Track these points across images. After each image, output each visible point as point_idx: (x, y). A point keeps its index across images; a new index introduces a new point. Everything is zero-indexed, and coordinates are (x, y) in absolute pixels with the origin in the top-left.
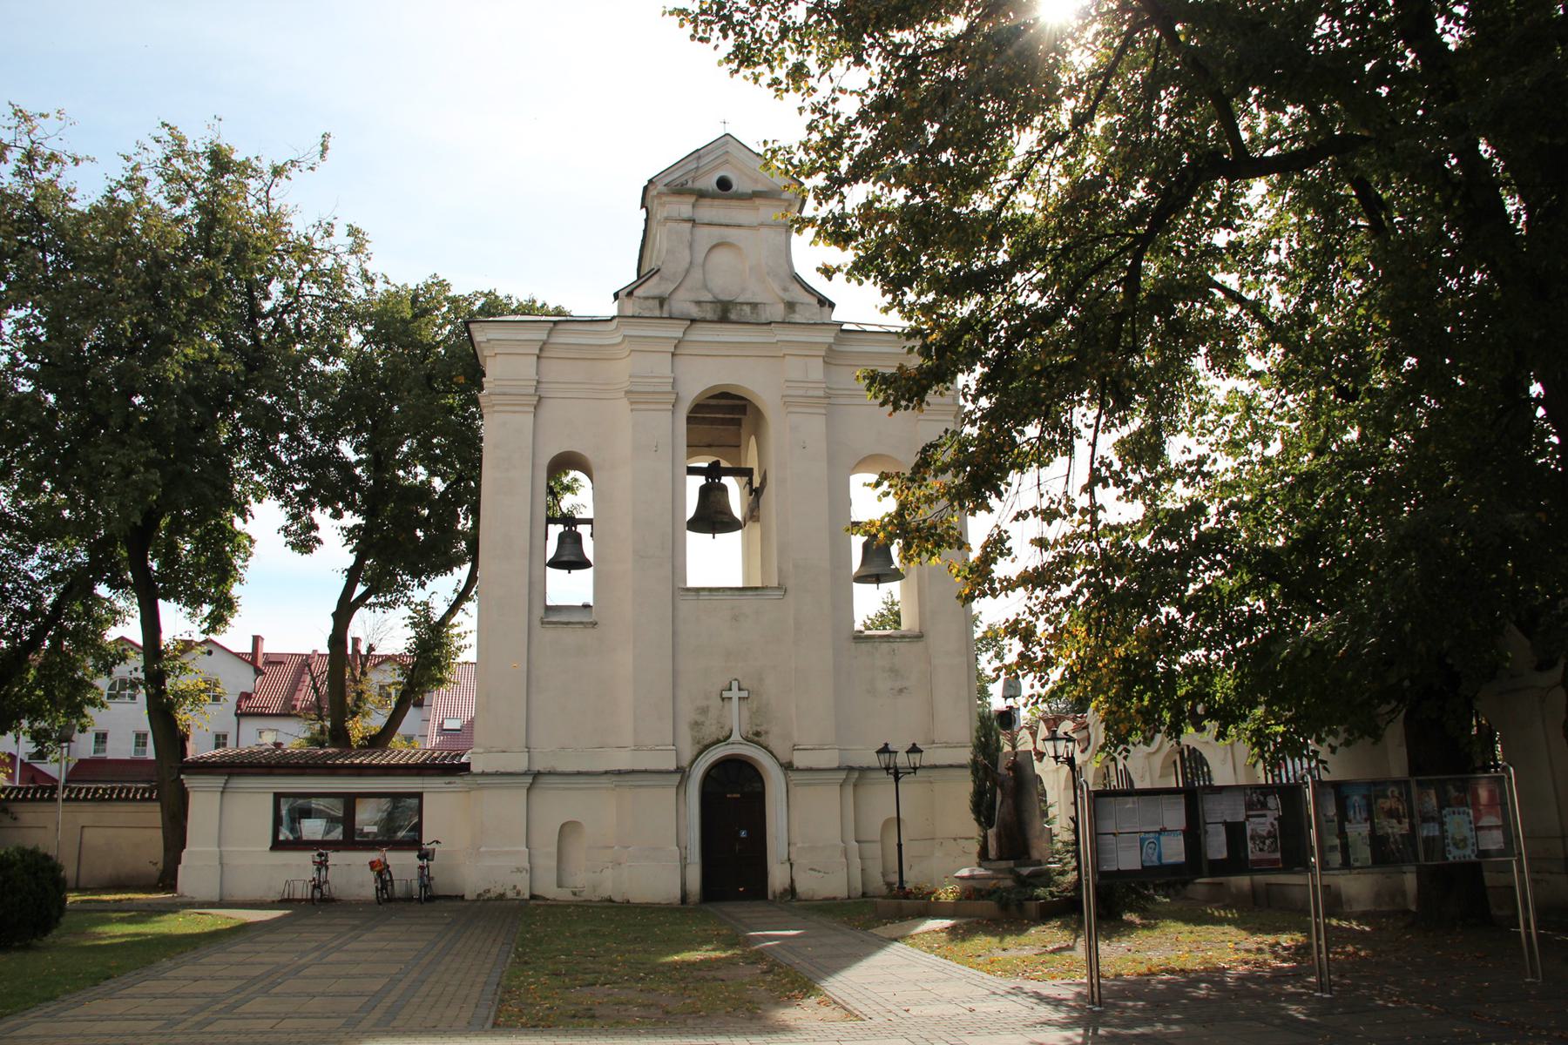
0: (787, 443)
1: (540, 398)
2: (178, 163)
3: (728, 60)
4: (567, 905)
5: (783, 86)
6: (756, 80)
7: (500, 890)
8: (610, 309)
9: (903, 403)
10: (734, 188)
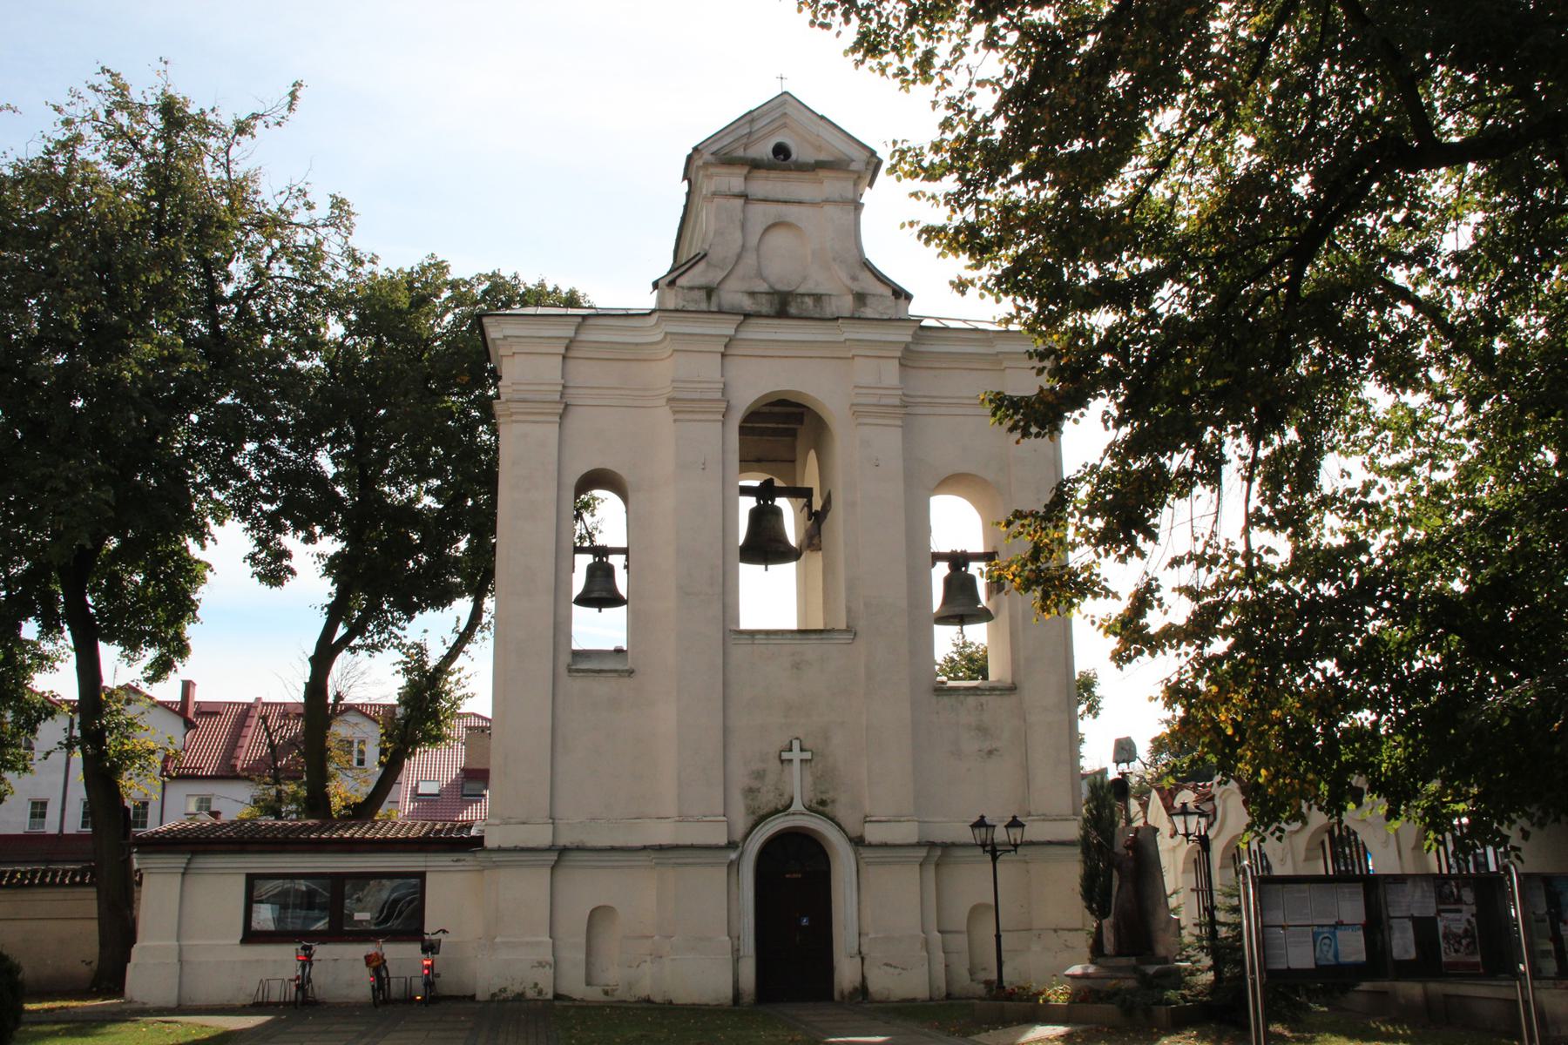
0: (857, 457)
1: (567, 405)
2: (123, 118)
3: (854, 49)
4: (599, 1007)
5: (910, 77)
6: (883, 71)
7: (517, 989)
8: (648, 301)
9: (1034, 430)
10: (794, 156)
